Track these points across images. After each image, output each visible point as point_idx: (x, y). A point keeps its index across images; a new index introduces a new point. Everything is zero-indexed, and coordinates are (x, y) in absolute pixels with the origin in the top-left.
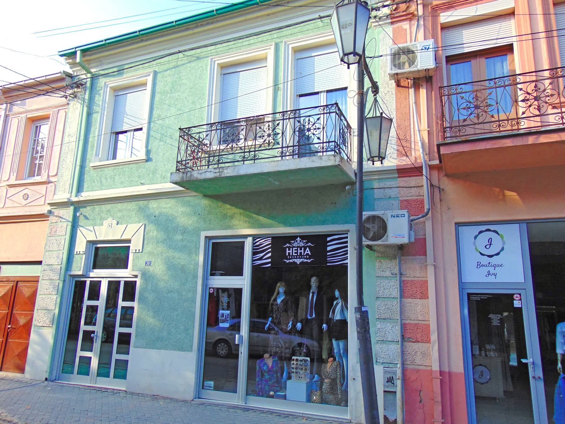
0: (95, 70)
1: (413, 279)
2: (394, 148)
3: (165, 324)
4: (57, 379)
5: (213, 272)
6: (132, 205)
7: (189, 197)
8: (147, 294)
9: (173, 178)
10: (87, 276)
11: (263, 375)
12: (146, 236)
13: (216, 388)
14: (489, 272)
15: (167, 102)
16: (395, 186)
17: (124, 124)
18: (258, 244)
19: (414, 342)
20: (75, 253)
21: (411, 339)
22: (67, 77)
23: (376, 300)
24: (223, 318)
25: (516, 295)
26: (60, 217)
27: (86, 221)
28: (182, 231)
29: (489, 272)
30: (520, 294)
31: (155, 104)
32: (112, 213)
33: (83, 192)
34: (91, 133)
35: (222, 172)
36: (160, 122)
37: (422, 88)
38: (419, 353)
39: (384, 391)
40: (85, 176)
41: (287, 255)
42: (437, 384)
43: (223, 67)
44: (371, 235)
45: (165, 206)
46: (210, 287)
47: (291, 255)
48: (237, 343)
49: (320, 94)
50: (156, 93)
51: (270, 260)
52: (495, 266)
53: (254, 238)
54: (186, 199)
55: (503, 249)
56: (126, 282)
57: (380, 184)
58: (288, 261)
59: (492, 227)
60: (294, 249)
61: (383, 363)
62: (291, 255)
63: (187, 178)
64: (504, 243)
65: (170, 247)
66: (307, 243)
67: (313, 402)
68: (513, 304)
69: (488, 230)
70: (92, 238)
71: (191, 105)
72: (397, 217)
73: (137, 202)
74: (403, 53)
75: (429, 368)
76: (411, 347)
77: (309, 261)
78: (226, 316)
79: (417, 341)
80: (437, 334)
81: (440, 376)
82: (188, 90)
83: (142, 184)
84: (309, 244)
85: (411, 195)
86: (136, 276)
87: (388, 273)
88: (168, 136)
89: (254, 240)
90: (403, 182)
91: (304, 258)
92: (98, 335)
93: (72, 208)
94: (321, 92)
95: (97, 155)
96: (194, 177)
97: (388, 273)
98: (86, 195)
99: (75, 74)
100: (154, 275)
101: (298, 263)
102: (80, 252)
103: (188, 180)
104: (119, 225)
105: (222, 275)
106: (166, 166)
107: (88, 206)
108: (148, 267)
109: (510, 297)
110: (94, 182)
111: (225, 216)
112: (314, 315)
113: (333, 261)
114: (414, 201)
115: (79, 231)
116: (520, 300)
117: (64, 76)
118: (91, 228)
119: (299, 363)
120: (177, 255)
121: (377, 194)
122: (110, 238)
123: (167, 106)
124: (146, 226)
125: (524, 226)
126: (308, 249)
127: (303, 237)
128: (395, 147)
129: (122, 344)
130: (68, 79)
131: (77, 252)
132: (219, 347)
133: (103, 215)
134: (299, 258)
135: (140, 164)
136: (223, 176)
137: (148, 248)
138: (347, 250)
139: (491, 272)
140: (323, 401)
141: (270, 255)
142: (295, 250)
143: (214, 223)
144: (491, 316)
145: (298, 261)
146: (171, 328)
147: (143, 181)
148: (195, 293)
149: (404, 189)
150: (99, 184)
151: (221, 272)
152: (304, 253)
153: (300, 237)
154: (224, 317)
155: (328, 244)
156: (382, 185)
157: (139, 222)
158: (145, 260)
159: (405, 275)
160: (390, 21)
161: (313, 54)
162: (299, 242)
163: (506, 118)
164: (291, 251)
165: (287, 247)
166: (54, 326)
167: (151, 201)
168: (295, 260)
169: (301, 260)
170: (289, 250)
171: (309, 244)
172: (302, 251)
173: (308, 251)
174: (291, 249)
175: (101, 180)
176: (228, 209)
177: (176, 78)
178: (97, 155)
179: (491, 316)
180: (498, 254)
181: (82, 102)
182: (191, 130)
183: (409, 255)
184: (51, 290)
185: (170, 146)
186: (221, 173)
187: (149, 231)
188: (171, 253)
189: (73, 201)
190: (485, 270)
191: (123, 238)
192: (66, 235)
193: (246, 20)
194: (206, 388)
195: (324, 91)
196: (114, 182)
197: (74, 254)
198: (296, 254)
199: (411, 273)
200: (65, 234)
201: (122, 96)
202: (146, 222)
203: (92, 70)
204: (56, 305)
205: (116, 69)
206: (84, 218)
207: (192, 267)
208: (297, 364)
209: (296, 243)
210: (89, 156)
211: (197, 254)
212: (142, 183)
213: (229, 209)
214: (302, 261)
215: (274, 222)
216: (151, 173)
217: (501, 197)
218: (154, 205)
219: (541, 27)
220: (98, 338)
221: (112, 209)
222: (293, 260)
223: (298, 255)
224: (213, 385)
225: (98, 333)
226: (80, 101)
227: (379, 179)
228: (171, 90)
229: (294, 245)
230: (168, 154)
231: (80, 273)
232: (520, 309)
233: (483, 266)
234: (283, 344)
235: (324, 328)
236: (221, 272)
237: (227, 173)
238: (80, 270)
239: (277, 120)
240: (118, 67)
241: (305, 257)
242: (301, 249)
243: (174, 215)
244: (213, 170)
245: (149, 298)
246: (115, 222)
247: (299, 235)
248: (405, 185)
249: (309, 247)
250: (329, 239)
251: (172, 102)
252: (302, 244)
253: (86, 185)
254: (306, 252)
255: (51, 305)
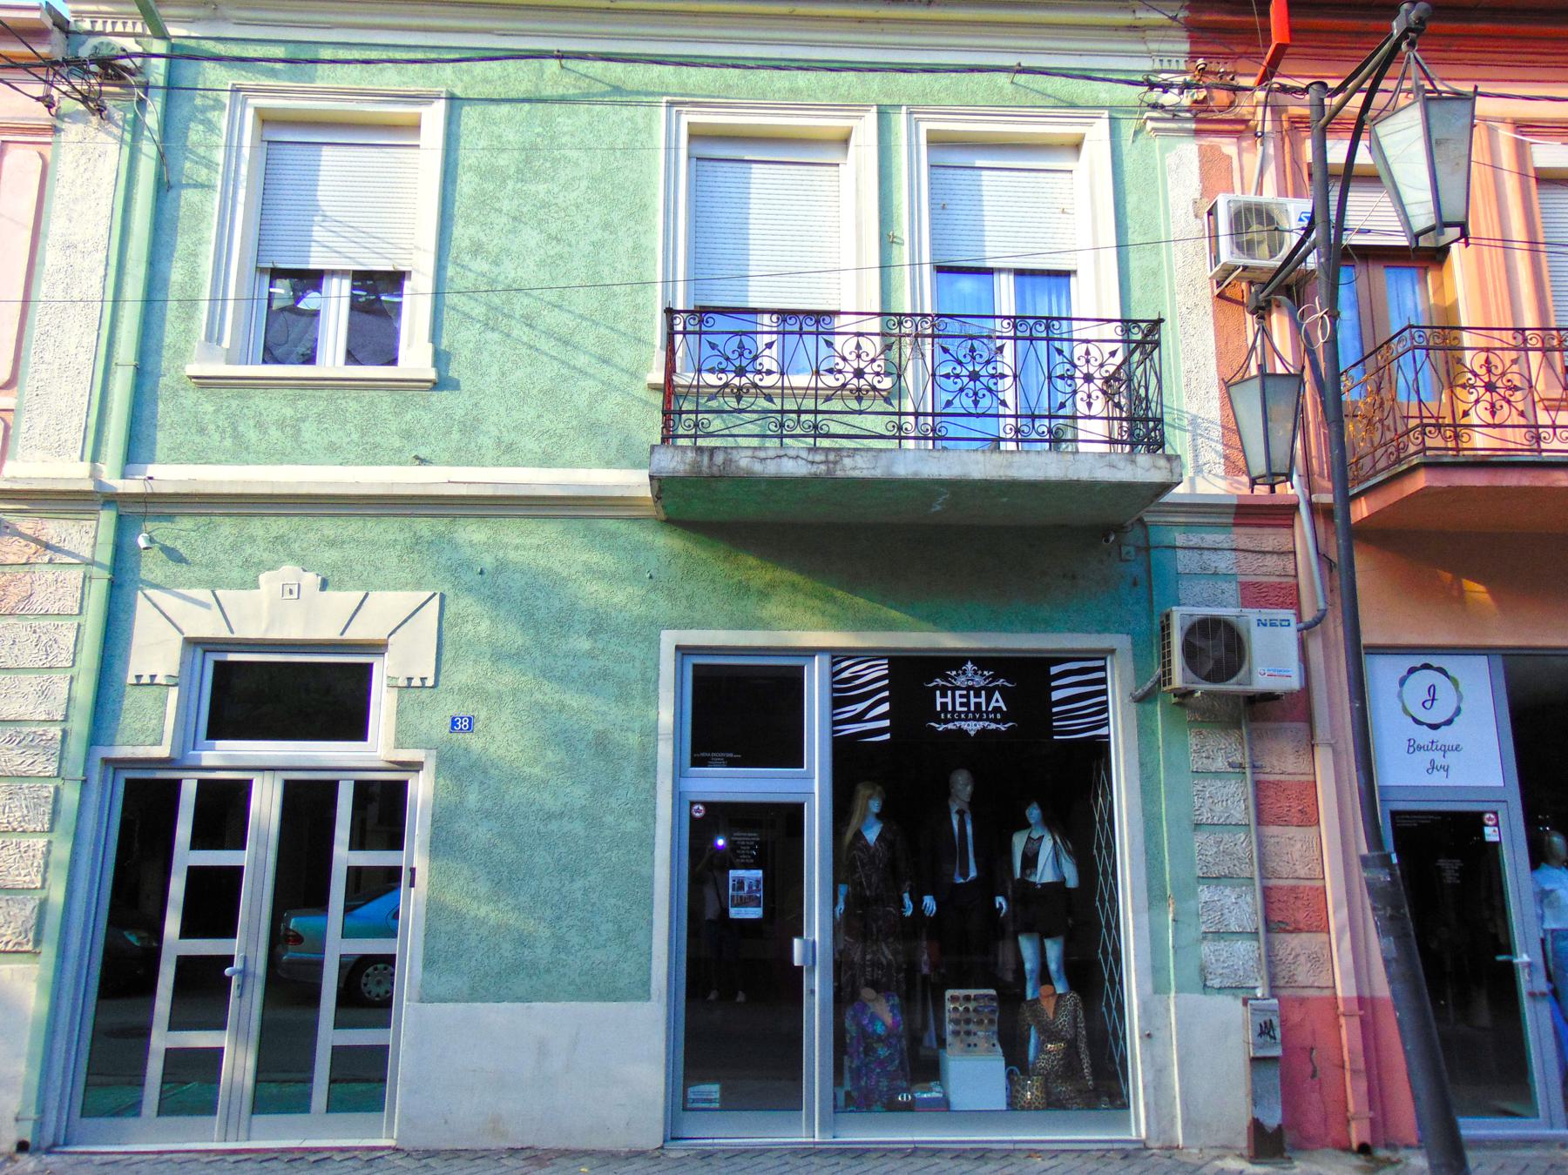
0: (184, 33)
1: (1278, 777)
2: (1216, 452)
3: (539, 918)
4: (61, 1142)
5: (703, 754)
6: (383, 526)
7: (611, 521)
8: (462, 825)
9: (663, 464)
10: (189, 763)
11: (869, 1050)
12: (448, 636)
13: (731, 1103)
14: (1433, 761)
15: (506, 206)
16: (1225, 546)
17: (315, 248)
18: (845, 675)
19: (1291, 932)
20: (131, 679)
21: (1283, 926)
22: (56, 29)
23: (1195, 830)
24: (741, 893)
25: (1487, 816)
26: (47, 546)
27: (172, 567)
28: (588, 625)
29: (1433, 761)
30: (1495, 813)
31: (457, 204)
32: (298, 550)
33: (152, 461)
34: (176, 255)
35: (835, 463)
36: (480, 265)
37: (1280, 313)
38: (1302, 959)
39: (1255, 1061)
40: (161, 406)
41: (939, 709)
42: (1349, 1034)
43: (698, 136)
44: (1210, 665)
45: (518, 541)
46: (694, 799)
47: (950, 708)
48: (797, 962)
49: (996, 277)
50: (460, 171)
51: (886, 723)
52: (1445, 750)
53: (833, 657)
54: (604, 524)
55: (1458, 711)
56: (362, 788)
57: (1191, 537)
58: (941, 728)
59: (1435, 661)
60: (958, 693)
61: (1220, 988)
62: (950, 708)
63: (715, 468)
64: (1460, 698)
65: (547, 673)
66: (995, 678)
67: (1023, 1108)
68: (1482, 834)
69: (1426, 666)
70: (209, 626)
71: (600, 232)
72: (1271, 625)
73: (407, 521)
74: (1509, 244)
75: (1327, 993)
76: (1291, 944)
77: (1002, 728)
78: (750, 887)
79: (1298, 930)
80: (1346, 910)
81: (1361, 1009)
82: (584, 183)
83: (422, 461)
84: (1001, 682)
85: (1269, 569)
86: (415, 767)
87: (1220, 764)
88: (517, 317)
89: (834, 664)
90: (1244, 537)
91: (988, 719)
92: (251, 969)
93: (107, 517)
94: (1000, 270)
95: (213, 336)
96: (738, 467)
97: (1220, 764)
98: (167, 475)
99: (86, 25)
100: (489, 763)
101: (972, 733)
102: (153, 677)
103: (717, 474)
104: (328, 593)
105: (731, 763)
106: (514, 413)
107: (183, 514)
108: (460, 736)
109: (1474, 821)
110: (202, 431)
111: (743, 590)
112: (973, 874)
113: (1070, 730)
114: (1272, 586)
115: (142, 604)
116: (1497, 825)
117: (49, 23)
118: (204, 594)
119: (971, 1006)
120: (574, 700)
121: (1185, 561)
122: (294, 632)
123: (504, 219)
124: (447, 601)
125: (1498, 662)
126: (997, 695)
127: (983, 661)
128: (1220, 448)
129: (1182, 992)
130: (57, 36)
131: (139, 677)
132: (368, 976)
133: (258, 552)
134: (974, 719)
135: (410, 393)
136: (839, 474)
137: (462, 674)
138: (1106, 702)
139: (1438, 763)
140: (1053, 1103)
141: (885, 707)
142: (961, 696)
143: (707, 607)
144: (1442, 862)
145: (972, 727)
146: (565, 930)
147: (423, 452)
148: (650, 820)
149: (1250, 556)
150: (228, 443)
151: (731, 755)
152: (987, 706)
153: (975, 661)
154: (746, 888)
155: (1053, 684)
156: (1194, 540)
157: (418, 585)
158: (454, 712)
159: (1262, 767)
160: (1194, 126)
161: (979, 163)
162: (969, 676)
163: (1550, 423)
164: (949, 700)
165: (937, 687)
166: (49, 951)
167: (462, 521)
168: (964, 725)
169: (979, 726)
170: (944, 695)
171: (1001, 682)
172: (983, 700)
173: (997, 701)
174: (949, 693)
175: (235, 429)
176: (750, 568)
177: (538, 135)
178: (213, 336)
179: (1442, 862)
180: (1449, 722)
181: (128, 137)
182: (711, 321)
183: (1268, 720)
184: (18, 814)
185: (524, 351)
186: (831, 466)
187: (462, 618)
188: (549, 693)
189: (120, 491)
190: (1424, 758)
191: (349, 635)
192: (80, 613)
193: (791, 17)
194: (696, 1105)
195: (1008, 271)
196: (296, 441)
197: (123, 685)
198: (965, 709)
199: (1275, 763)
200: (76, 611)
201: (289, 146)
202: (446, 588)
203: (173, 30)
204: (45, 871)
205: (279, 52)
206: (163, 556)
207: (633, 739)
208: (967, 1010)
209: (963, 678)
210: (171, 333)
211: (651, 698)
212: (422, 456)
213: (756, 571)
214: (984, 729)
215: (903, 615)
216: (455, 428)
217: (1455, 593)
218: (472, 534)
219: (1517, 230)
220: (249, 980)
221: (293, 535)
222: (958, 724)
223: (969, 711)
224: (717, 1096)
225: (251, 963)
226: (117, 131)
227: (1186, 525)
228: (519, 171)
229: (959, 684)
230: (519, 373)
231: (163, 751)
232: (1496, 845)
233: (1420, 748)
234: (890, 957)
235: (1001, 907)
236: (731, 755)
237: (854, 469)
238: (159, 743)
239: (998, 338)
240: (292, 47)
241: (991, 716)
242: (978, 695)
243: (557, 574)
244: (804, 454)
245: (474, 837)
246: (311, 580)
247: (972, 655)
248: (1250, 546)
249: (1002, 690)
250: (1054, 670)
251: (525, 210)
252: (979, 681)
253: (163, 440)
254: (993, 704)
255: (23, 872)
